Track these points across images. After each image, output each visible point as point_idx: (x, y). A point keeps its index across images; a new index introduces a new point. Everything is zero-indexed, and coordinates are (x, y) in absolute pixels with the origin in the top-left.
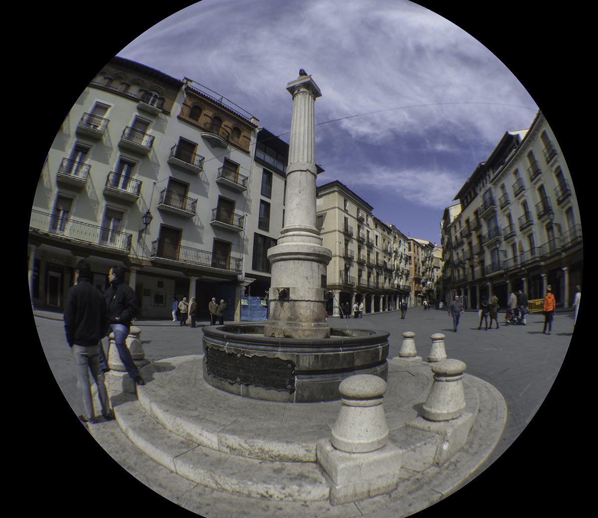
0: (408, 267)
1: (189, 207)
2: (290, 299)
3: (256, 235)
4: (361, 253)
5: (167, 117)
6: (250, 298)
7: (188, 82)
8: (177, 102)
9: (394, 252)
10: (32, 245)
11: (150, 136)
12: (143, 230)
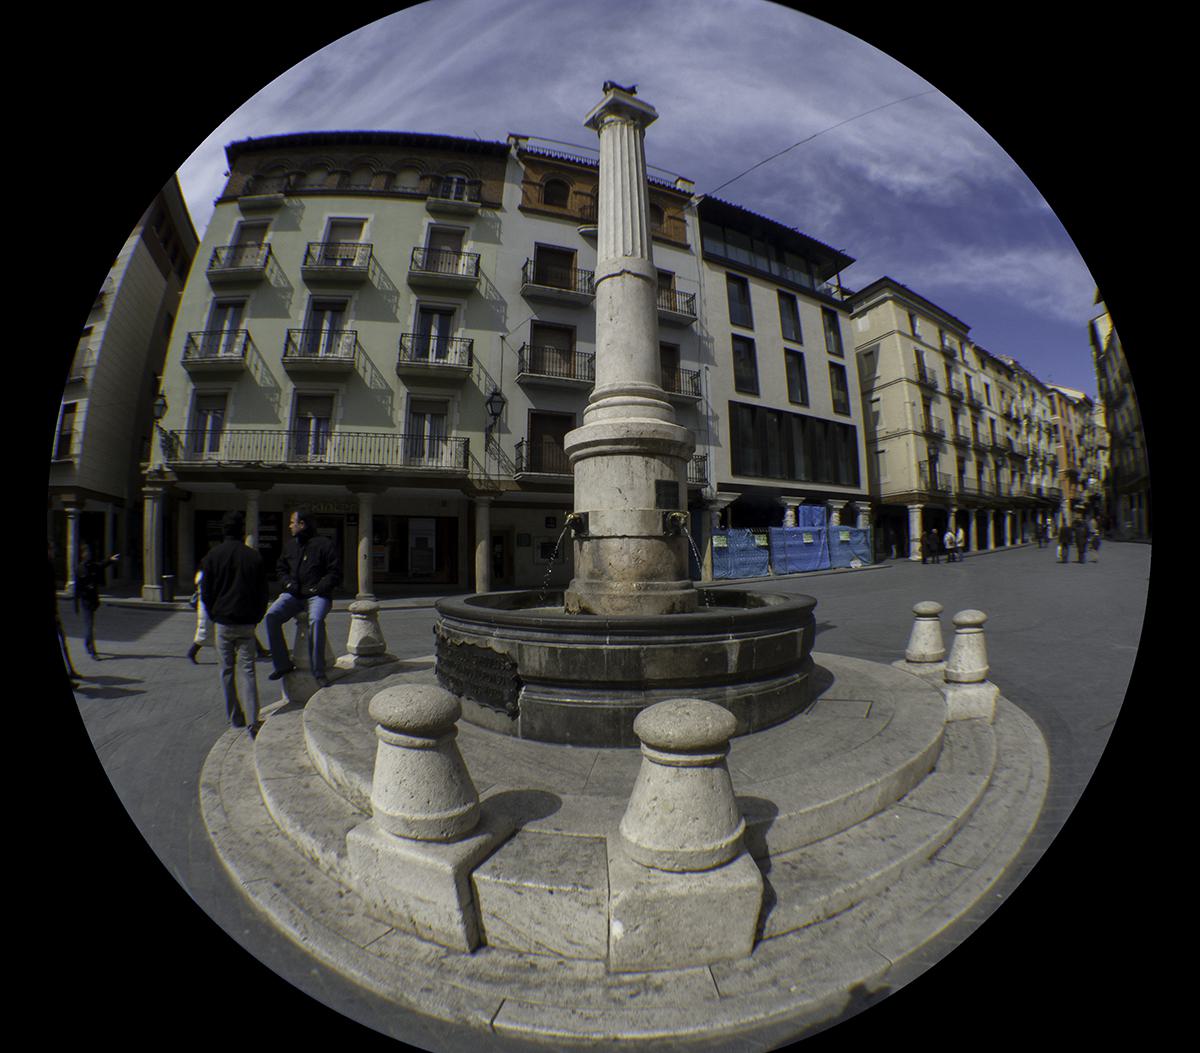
0: (1054, 449)
1: (581, 372)
2: (590, 535)
3: (733, 405)
4: (960, 423)
5: (498, 213)
6: (731, 532)
7: (521, 141)
8: (509, 182)
9: (1026, 416)
10: (249, 491)
11: (469, 254)
12: (491, 427)
